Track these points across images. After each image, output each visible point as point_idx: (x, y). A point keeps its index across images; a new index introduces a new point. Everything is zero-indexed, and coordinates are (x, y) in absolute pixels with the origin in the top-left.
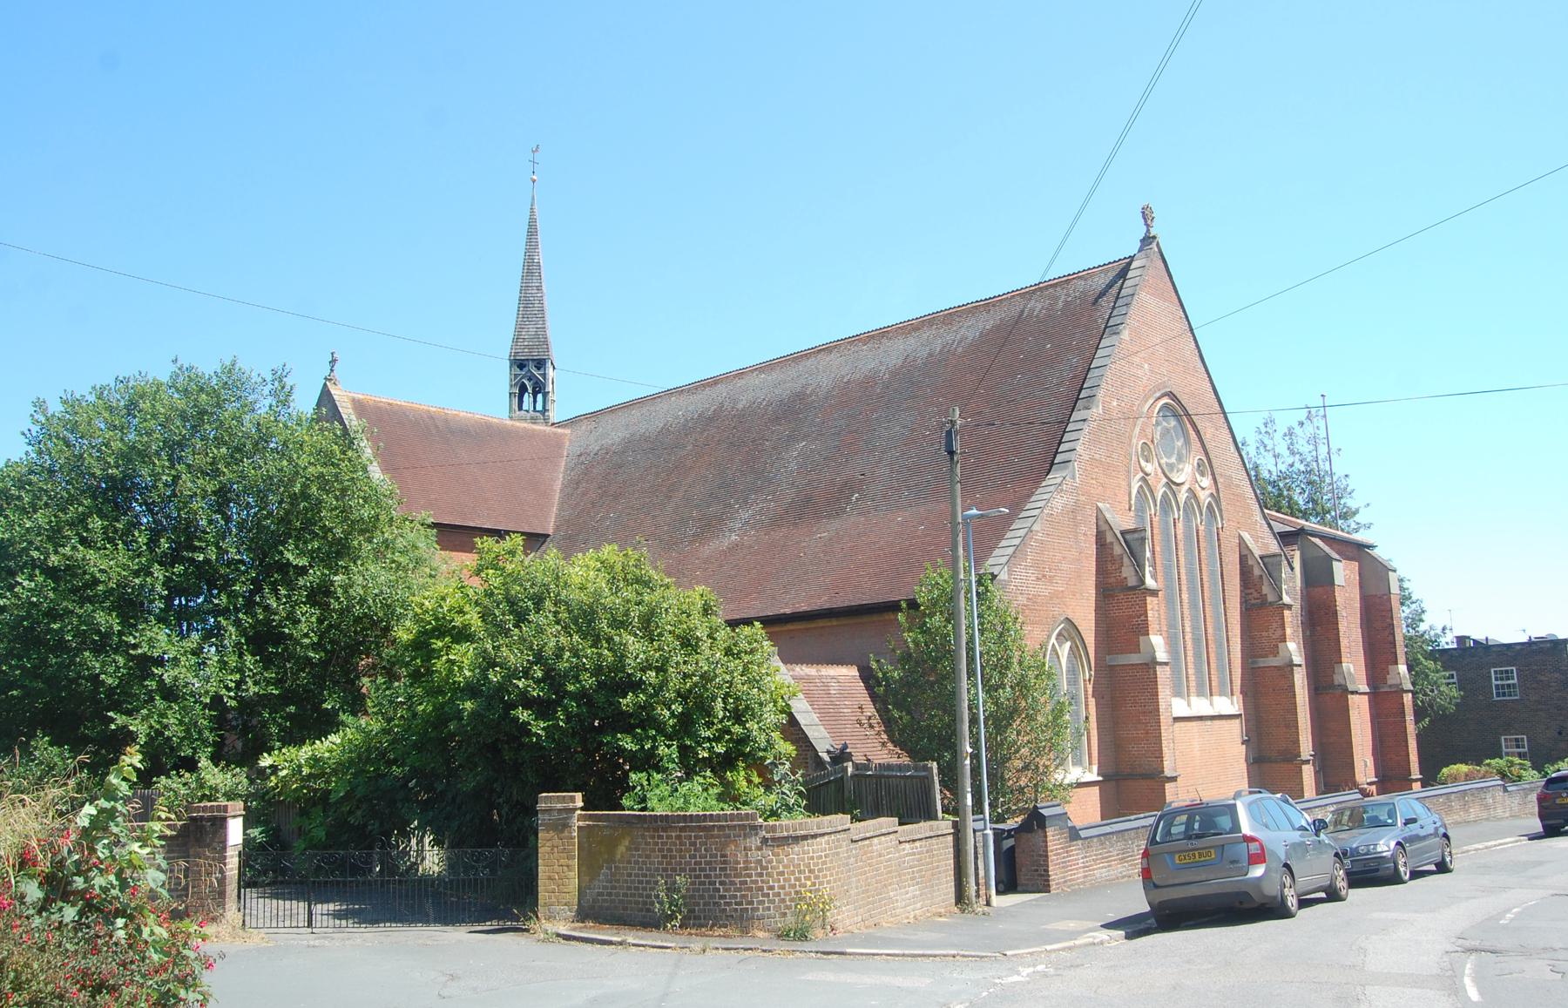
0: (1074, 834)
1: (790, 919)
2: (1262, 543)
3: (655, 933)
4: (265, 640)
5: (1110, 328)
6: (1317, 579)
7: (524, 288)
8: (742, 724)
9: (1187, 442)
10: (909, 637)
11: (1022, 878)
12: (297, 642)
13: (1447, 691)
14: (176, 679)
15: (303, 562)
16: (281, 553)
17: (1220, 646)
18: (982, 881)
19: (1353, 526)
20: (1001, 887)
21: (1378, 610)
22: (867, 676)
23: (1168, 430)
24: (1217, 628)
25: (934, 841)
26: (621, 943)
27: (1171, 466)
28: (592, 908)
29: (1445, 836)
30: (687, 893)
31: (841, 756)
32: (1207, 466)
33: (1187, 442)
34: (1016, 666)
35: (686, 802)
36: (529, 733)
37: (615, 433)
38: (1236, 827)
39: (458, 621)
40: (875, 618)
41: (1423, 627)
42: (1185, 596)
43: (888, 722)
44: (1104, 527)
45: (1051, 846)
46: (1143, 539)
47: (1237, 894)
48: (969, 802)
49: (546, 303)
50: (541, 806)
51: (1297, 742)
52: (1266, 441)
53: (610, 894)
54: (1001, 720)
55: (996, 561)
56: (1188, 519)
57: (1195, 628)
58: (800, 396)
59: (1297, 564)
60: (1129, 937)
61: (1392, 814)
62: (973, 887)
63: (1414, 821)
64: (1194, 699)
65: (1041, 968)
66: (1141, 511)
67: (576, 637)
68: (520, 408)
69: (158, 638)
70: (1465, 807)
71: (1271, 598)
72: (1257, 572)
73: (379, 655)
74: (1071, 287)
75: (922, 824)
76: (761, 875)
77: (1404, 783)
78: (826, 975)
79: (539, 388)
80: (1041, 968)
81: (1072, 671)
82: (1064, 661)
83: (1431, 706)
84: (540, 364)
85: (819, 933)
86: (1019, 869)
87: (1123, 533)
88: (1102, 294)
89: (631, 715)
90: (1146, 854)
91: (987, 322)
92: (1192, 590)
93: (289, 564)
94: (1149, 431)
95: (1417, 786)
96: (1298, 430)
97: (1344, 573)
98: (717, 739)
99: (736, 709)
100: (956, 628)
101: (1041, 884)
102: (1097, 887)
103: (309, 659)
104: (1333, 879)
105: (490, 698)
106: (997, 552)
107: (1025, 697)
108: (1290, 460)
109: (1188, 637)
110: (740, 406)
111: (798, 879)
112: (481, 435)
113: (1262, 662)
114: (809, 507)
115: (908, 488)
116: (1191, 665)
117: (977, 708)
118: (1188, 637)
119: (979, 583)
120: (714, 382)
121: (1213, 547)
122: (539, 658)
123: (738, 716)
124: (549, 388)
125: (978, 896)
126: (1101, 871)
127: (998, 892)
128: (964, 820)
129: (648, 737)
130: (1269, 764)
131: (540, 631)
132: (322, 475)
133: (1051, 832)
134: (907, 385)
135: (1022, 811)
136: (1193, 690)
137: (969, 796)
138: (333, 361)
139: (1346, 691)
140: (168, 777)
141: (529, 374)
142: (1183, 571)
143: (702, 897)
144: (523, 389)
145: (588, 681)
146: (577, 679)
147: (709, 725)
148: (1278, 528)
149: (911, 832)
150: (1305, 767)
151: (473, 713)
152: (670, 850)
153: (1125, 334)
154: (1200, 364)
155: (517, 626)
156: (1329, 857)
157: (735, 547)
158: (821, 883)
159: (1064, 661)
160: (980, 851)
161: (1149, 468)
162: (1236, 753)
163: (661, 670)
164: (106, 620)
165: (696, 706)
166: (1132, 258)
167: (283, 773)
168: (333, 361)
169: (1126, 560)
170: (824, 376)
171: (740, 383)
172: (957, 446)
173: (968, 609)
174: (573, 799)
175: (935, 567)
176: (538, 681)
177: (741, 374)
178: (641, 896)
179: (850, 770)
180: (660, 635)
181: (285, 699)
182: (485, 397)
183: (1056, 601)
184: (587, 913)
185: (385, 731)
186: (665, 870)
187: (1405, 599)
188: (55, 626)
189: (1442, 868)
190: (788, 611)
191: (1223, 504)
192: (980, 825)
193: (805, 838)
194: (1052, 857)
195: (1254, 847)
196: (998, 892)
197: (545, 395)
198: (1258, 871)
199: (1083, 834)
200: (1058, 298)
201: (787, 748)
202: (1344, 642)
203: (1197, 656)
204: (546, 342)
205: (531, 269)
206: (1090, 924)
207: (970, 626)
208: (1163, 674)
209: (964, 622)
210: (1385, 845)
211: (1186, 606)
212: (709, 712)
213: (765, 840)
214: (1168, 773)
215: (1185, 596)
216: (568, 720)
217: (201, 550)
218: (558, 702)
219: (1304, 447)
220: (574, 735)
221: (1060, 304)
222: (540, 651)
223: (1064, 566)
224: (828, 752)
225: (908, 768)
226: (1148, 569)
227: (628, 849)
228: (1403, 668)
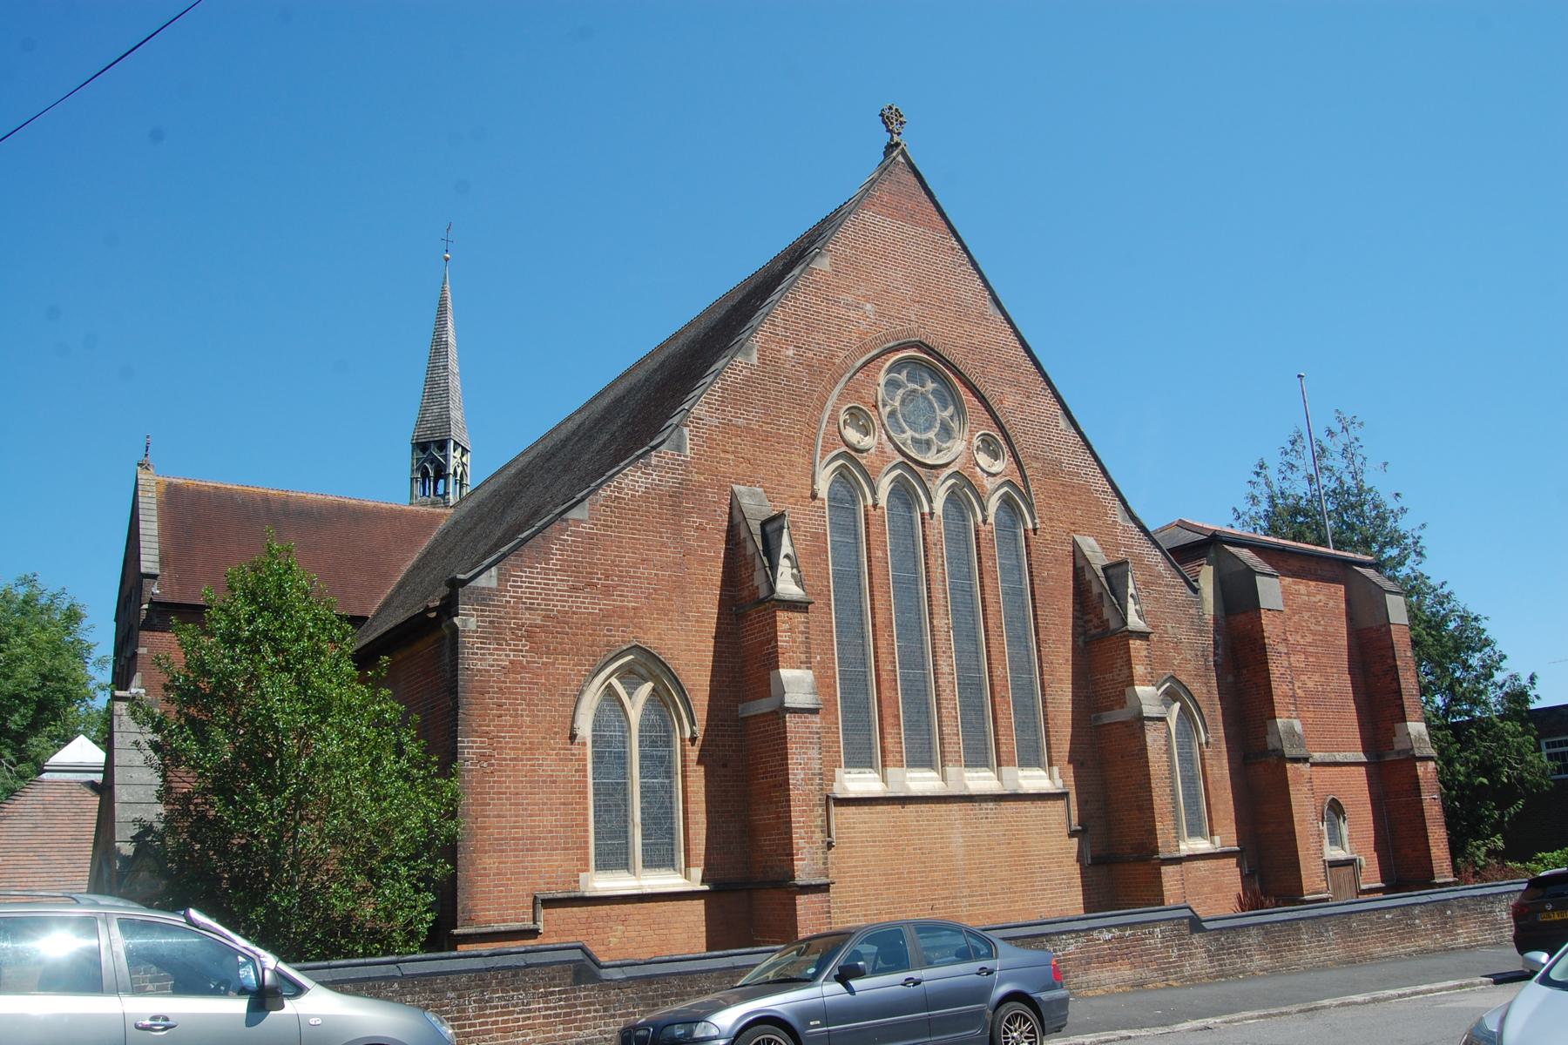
9: (960, 410)
33: (960, 410)
70: (1446, 926)
71: (1113, 625)
72: (1096, 589)
139: (1282, 759)
141: (430, 457)
144: (425, 475)
154: (992, 310)
182: (387, 485)
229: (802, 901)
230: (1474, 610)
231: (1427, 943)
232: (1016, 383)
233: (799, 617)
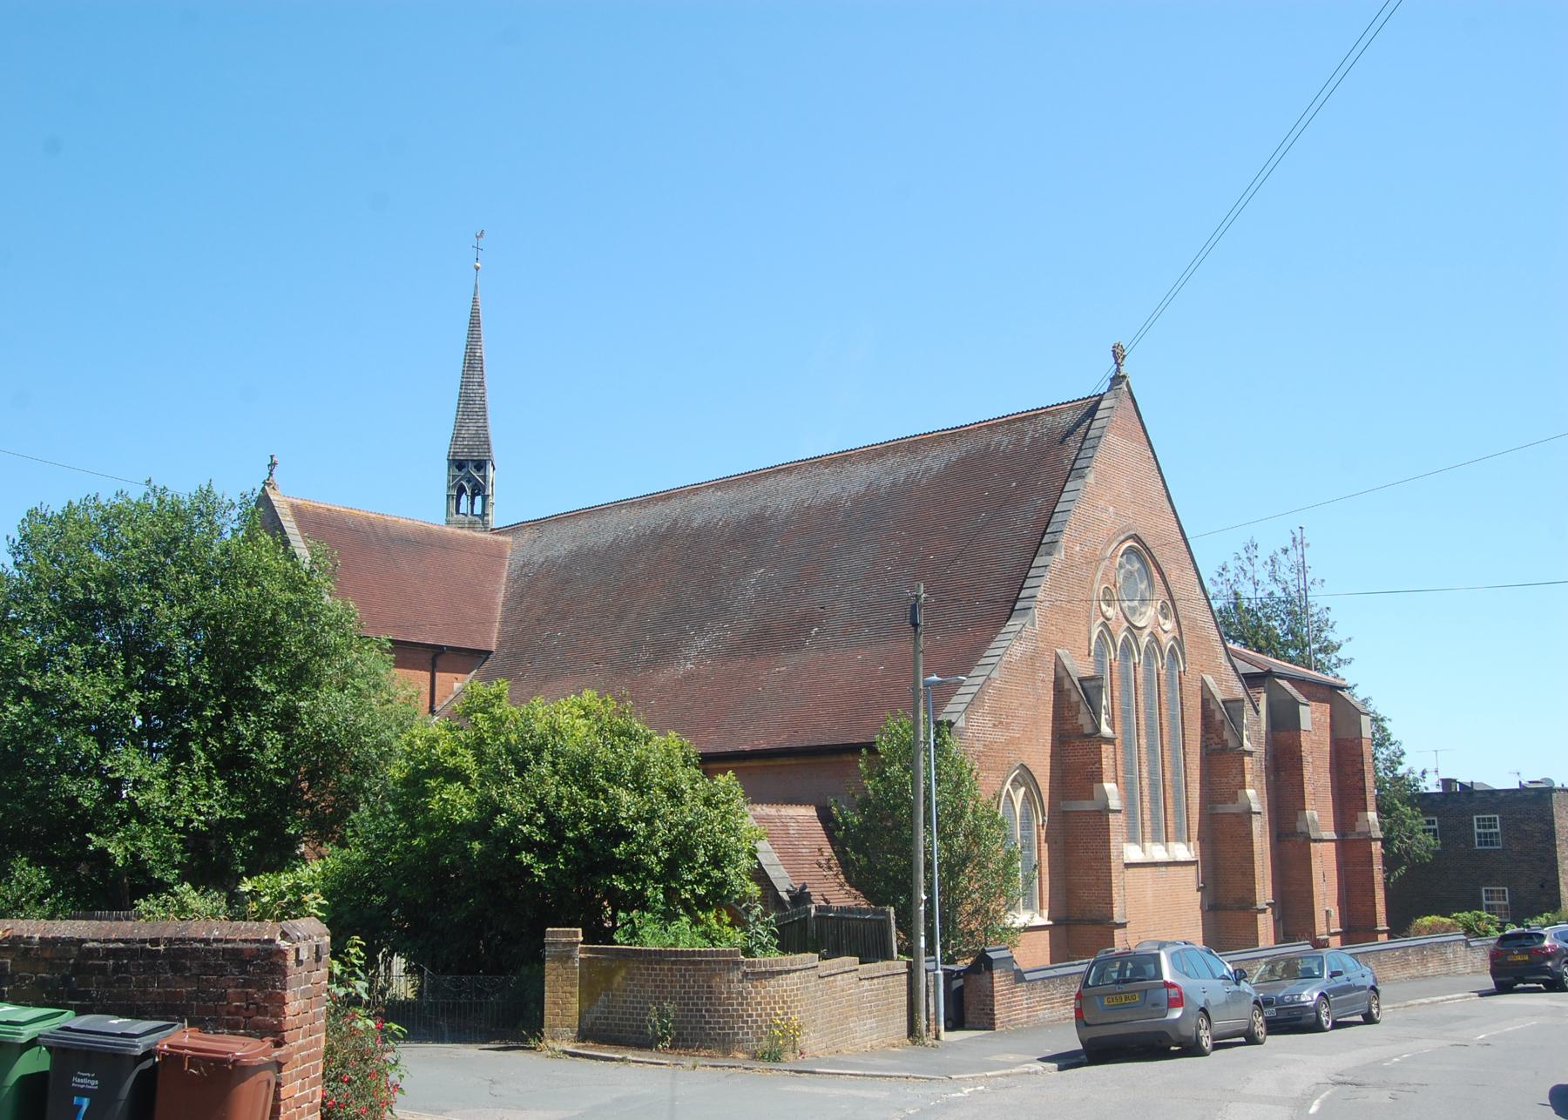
0: (1019, 977)
1: (765, 1043)
2: (1225, 686)
3: (648, 1052)
4: (231, 763)
5: (1075, 471)
6: (1283, 723)
7: (465, 385)
8: (721, 869)
9: (1151, 584)
10: (869, 784)
11: (969, 1017)
13: (1423, 840)
14: (148, 803)
16: (249, 679)
17: (1178, 791)
20: (950, 1024)
22: (825, 817)
23: (1131, 573)
24: (1176, 773)
26: (622, 1060)
27: (1133, 610)
28: (591, 1030)
29: (1373, 988)
31: (801, 897)
32: (1171, 607)
33: (1151, 584)
34: (969, 816)
35: (677, 939)
37: (561, 545)
38: (1159, 974)
40: (834, 759)
41: (1401, 770)
42: (1143, 741)
43: (845, 865)
45: (997, 986)
46: (1101, 687)
48: (923, 944)
49: (488, 399)
50: (548, 939)
52: (1247, 567)
54: (953, 868)
55: (953, 711)
56: (1148, 664)
57: (1152, 773)
58: (758, 519)
60: (1060, 1069)
61: (1321, 967)
62: (924, 1022)
63: (1340, 973)
66: (1100, 655)
67: (575, 788)
69: (129, 762)
70: (1423, 961)
71: (1231, 744)
72: (1218, 716)
73: (339, 780)
75: (879, 963)
77: (1370, 933)
79: (479, 490)
81: (1026, 816)
83: (1408, 853)
84: (480, 465)
85: (791, 1056)
86: (967, 1007)
87: (1080, 680)
88: (1070, 433)
89: (623, 862)
90: (1079, 996)
93: (256, 689)
95: (1383, 938)
96: (1282, 557)
97: (1313, 718)
98: (699, 882)
99: (715, 855)
101: (986, 1022)
103: (272, 784)
104: (1252, 1024)
106: (955, 699)
107: (977, 844)
109: (1145, 782)
110: (695, 525)
112: (420, 543)
113: (1221, 809)
114: (768, 639)
116: (1146, 811)
117: (932, 854)
118: (1145, 782)
119: (938, 734)
123: (716, 862)
125: (928, 1030)
126: (1040, 1012)
127: (947, 1029)
130: (1225, 916)
131: (542, 780)
132: (290, 603)
135: (971, 953)
136: (1148, 835)
138: (273, 465)
139: (1308, 840)
140: (146, 900)
141: (469, 472)
142: (1142, 716)
145: (586, 829)
146: (575, 826)
147: (691, 869)
148: (1245, 668)
151: (481, 853)
153: (1091, 478)
155: (519, 774)
156: (1247, 1006)
157: (689, 677)
161: (1110, 612)
162: (1191, 900)
163: (649, 822)
164: (87, 745)
166: (1101, 396)
168: (273, 465)
169: (1082, 707)
170: (784, 498)
171: (695, 499)
172: (921, 620)
173: (926, 763)
174: (576, 934)
175: (895, 715)
176: (540, 827)
177: (696, 489)
180: (649, 788)
182: (417, 499)
184: (584, 1035)
187: (1383, 740)
188: (40, 751)
189: (1369, 1019)
190: (747, 748)
191: (1186, 647)
192: (931, 966)
193: (780, 973)
194: (998, 997)
195: (1173, 992)
196: (947, 1029)
197: (485, 498)
198: (1176, 1014)
199: (1027, 977)
203: (1154, 800)
204: (487, 442)
206: (1028, 1058)
207: (928, 777)
209: (922, 774)
211: (1143, 751)
212: (691, 857)
213: (745, 974)
214: (1117, 919)
215: (1143, 741)
216: (567, 861)
217: (174, 675)
218: (558, 846)
219: (1284, 574)
221: (1028, 440)
223: (1022, 712)
225: (867, 911)
227: (624, 979)
228: (1372, 815)
229: (1116, 932)
230: (1381, 712)
231: (1413, 971)
232: (1176, 561)
233: (1111, 748)
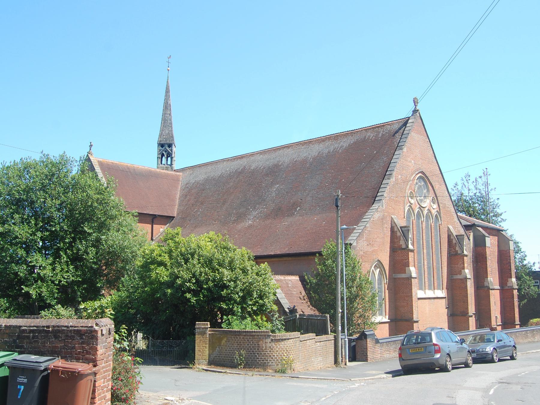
0: (377, 341)
1: (280, 366)
2: (457, 230)
3: (235, 370)
4: (76, 259)
5: (398, 147)
6: (479, 244)
7: (164, 114)
8: (263, 300)
11: (358, 357)
12: (88, 261)
14: (45, 275)
15: (91, 231)
16: (82, 227)
17: (438, 270)
18: (343, 357)
19: (500, 220)
20: (350, 359)
21: (504, 257)
22: (303, 280)
23: (420, 186)
24: (438, 263)
25: (327, 342)
26: (225, 372)
27: (421, 200)
29: (514, 346)
30: (244, 357)
31: (293, 311)
32: (436, 199)
34: (358, 280)
35: (246, 326)
36: (190, 302)
37: (201, 176)
38: (431, 340)
39: (159, 259)
40: (306, 258)
41: (525, 262)
42: (425, 251)
43: (310, 298)
44: (394, 225)
45: (369, 345)
46: (408, 230)
47: (430, 363)
48: (340, 329)
50: (197, 326)
51: (467, 308)
53: (219, 357)
54: (352, 299)
55: (352, 239)
56: (427, 221)
57: (428, 263)
58: (276, 166)
59: (471, 238)
60: (393, 377)
61: (494, 338)
63: (501, 340)
64: (427, 291)
65: (362, 384)
66: (408, 217)
67: (207, 269)
68: (161, 164)
69: (37, 259)
70: (533, 336)
71: (459, 252)
72: (454, 242)
73: (117, 266)
74: (385, 128)
75: (323, 336)
76: (270, 351)
77: (513, 325)
78: (294, 383)
79: (169, 155)
80: (362, 384)
82: (377, 276)
83: (527, 294)
84: (170, 146)
85: (289, 371)
86: (357, 353)
87: (401, 227)
88: (397, 132)
89: (225, 297)
90: (400, 349)
91: (351, 140)
92: (428, 248)
93: (85, 232)
94: (413, 187)
95: (518, 327)
96: (479, 180)
97: (491, 242)
98: (254, 305)
99: (261, 294)
100: (337, 266)
101: (365, 359)
102: (385, 360)
103: (92, 267)
105: (177, 289)
106: (352, 235)
108: (475, 192)
109: (426, 267)
110: (252, 168)
111: (283, 353)
112: (147, 176)
113: (456, 277)
114: (280, 212)
115: (319, 206)
116: (426, 278)
117: (343, 294)
118: (426, 267)
120: (241, 157)
121: (437, 232)
122: (194, 276)
123: (261, 297)
124: (173, 156)
125: (342, 362)
126: (385, 354)
127: (349, 361)
128: (338, 335)
129: (231, 304)
130: (456, 318)
131: (194, 265)
133: (368, 340)
134: (319, 164)
135: (358, 332)
136: (427, 287)
137: (340, 327)
139: (489, 289)
140: (44, 311)
141: (166, 149)
142: (424, 241)
143: (251, 358)
144: (163, 155)
145: (211, 284)
146: (207, 283)
147: (251, 300)
148: (465, 223)
149: (320, 338)
150: (470, 318)
151: (171, 294)
152: (240, 342)
157: (250, 226)
158: (290, 355)
159: (377, 276)
160: (343, 346)
161: (412, 201)
163: (235, 282)
164: (21, 252)
165: (247, 293)
166: (409, 118)
167: (89, 311)
168: (91, 146)
169: (402, 238)
170: (286, 158)
171: (252, 158)
174: (207, 324)
175: (329, 241)
176: (194, 284)
177: (252, 154)
178: (230, 357)
179: (298, 316)
181: (83, 283)
182: (146, 159)
183: (374, 253)
184: (211, 362)
185: (127, 297)
186: (238, 349)
189: (512, 358)
190: (272, 253)
191: (442, 215)
192: (343, 337)
193: (285, 339)
194: (369, 349)
195: (437, 347)
196: (349, 361)
197: (172, 158)
198: (438, 356)
199: (380, 341)
200: (379, 132)
201: (275, 308)
202: (489, 269)
203: (429, 274)
204: (172, 137)
205: (167, 107)
206: (381, 372)
207: (342, 265)
208: (414, 282)
209: (340, 264)
210: (489, 349)
211: (425, 255)
212: (251, 295)
213: (272, 340)
214: (415, 319)
215: (425, 251)
218: (200, 291)
220: (205, 302)
221: (380, 135)
222: (194, 273)
223: (378, 240)
224: (288, 308)
225: (318, 316)
226: (410, 242)
227: (226, 342)
228: (514, 280)
230: (518, 240)
